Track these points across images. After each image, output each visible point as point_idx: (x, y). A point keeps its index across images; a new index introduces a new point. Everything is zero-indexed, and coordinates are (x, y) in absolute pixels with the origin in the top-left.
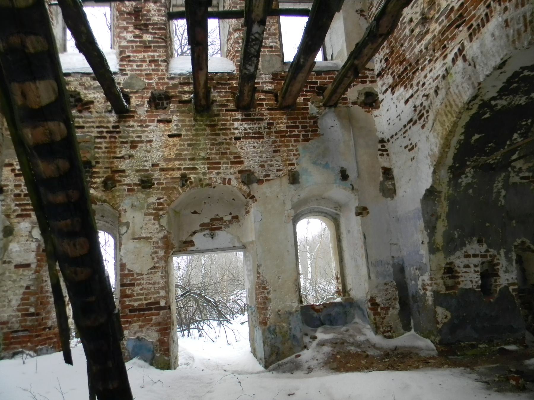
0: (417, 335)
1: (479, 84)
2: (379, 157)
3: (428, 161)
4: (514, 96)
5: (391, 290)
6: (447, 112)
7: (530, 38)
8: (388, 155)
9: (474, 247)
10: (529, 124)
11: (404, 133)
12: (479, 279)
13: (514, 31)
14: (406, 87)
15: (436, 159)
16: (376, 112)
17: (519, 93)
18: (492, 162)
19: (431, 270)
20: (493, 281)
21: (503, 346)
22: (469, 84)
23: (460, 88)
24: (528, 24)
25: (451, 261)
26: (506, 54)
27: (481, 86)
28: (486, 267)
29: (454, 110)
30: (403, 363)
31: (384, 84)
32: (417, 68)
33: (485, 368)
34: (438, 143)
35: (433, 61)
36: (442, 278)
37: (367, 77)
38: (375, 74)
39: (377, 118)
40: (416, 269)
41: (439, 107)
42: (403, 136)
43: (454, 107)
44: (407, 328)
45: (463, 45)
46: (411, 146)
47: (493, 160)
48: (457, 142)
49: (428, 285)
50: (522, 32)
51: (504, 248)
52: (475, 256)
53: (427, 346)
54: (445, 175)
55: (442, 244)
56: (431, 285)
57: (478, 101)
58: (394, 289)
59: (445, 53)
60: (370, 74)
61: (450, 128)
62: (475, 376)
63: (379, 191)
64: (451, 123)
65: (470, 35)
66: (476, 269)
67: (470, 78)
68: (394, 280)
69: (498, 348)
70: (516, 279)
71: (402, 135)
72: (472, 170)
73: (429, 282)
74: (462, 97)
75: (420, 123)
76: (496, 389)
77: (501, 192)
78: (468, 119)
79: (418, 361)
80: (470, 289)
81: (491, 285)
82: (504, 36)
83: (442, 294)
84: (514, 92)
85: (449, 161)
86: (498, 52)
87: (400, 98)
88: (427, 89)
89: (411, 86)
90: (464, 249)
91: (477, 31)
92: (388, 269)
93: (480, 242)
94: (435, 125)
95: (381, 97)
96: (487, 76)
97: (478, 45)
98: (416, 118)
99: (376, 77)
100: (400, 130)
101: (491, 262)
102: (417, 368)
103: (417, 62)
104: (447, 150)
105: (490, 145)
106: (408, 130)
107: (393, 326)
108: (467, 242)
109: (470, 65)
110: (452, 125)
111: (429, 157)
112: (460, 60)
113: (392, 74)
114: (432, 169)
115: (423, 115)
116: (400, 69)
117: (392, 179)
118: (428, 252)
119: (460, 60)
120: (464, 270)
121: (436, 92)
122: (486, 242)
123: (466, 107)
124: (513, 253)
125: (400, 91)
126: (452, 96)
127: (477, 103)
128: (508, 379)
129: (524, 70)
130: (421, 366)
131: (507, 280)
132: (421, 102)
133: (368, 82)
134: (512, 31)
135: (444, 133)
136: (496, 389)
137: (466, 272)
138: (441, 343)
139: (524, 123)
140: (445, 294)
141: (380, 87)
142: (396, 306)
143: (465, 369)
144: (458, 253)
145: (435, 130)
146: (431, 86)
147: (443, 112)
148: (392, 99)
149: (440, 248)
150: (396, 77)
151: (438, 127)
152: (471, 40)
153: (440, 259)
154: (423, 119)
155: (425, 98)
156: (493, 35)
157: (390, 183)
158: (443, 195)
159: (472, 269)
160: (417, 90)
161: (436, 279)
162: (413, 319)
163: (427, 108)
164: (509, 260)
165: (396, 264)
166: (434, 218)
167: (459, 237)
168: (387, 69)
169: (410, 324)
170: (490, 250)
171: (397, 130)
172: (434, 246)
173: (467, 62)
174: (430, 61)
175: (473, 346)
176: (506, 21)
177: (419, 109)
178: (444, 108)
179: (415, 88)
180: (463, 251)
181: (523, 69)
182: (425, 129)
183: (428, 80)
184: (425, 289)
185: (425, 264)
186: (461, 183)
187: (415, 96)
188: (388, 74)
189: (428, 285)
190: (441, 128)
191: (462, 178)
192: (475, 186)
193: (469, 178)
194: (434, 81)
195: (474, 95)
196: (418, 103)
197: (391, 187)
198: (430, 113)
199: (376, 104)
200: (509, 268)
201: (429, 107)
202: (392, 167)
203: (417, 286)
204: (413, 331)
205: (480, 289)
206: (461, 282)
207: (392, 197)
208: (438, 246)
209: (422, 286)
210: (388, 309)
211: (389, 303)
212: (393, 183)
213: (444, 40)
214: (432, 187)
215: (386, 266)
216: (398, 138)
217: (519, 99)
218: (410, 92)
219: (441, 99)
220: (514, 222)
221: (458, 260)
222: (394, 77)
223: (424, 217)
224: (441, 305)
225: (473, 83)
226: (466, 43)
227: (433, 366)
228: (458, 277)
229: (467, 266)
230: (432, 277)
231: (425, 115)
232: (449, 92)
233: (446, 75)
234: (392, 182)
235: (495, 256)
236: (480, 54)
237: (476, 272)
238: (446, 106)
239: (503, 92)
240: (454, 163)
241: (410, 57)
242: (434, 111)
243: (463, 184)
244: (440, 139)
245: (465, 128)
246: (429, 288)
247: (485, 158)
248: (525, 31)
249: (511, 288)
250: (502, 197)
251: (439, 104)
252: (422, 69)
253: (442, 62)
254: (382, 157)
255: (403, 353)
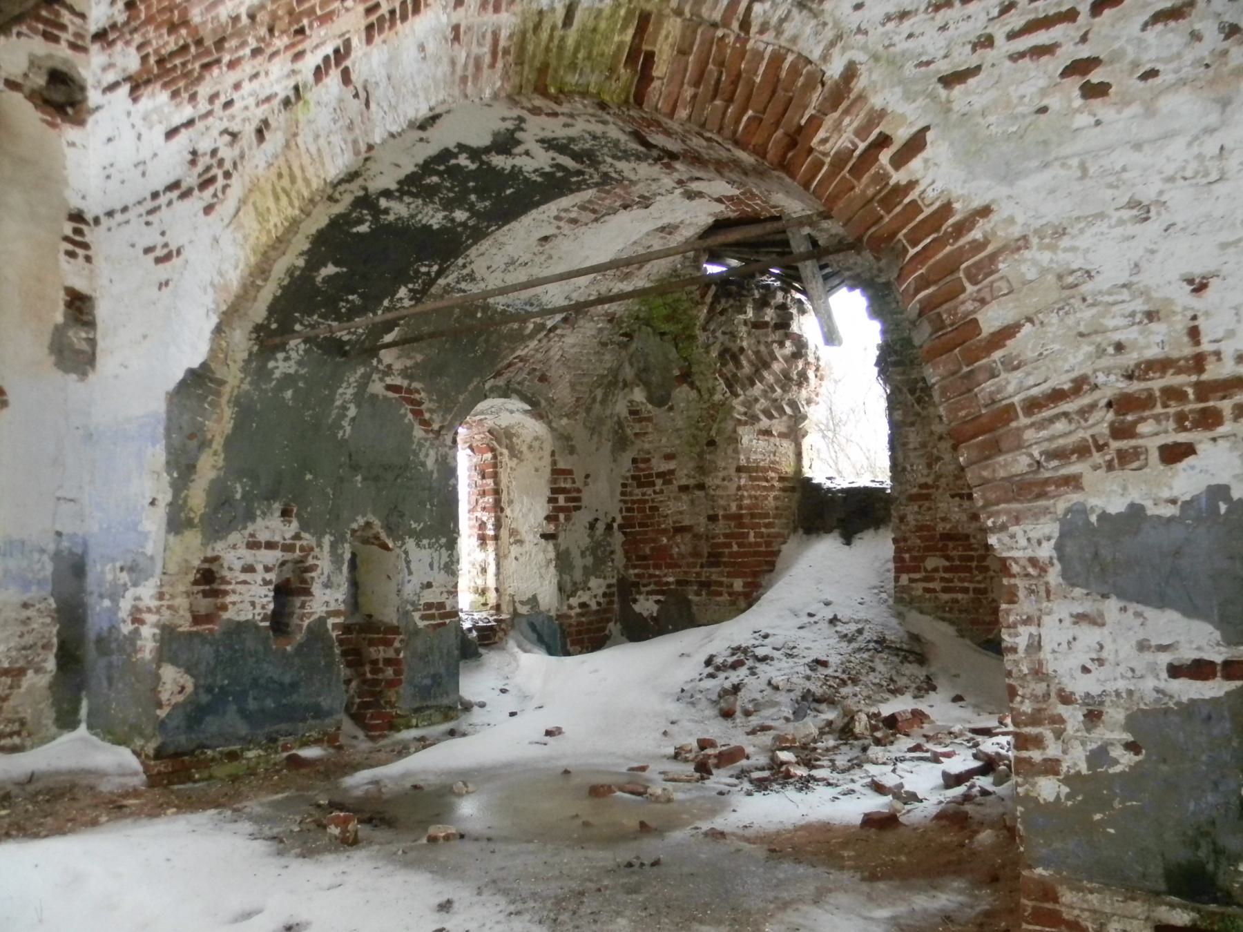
0: (94, 738)
1: (370, 147)
2: (63, 258)
3: (208, 300)
4: (425, 204)
5: (41, 620)
6: (279, 190)
7: (499, 84)
8: (88, 259)
9: (271, 526)
10: (433, 274)
11: (150, 212)
12: (270, 599)
13: (468, 56)
14: (175, 94)
15: (231, 299)
16: (71, 133)
17: (437, 200)
18: (346, 338)
19: (164, 573)
20: (298, 605)
21: (294, 752)
22: (345, 141)
23: (322, 141)
24: (500, 54)
25: (216, 553)
26: (444, 102)
27: (373, 153)
28: (288, 573)
29: (298, 192)
30: (51, 814)
31: (111, 66)
32: (215, 56)
33: (262, 805)
34: (242, 259)
35: (266, 55)
36: (188, 594)
37: (63, 27)
38: (87, 30)
39: (72, 149)
40: (122, 569)
41: (260, 171)
42: (145, 218)
43: (300, 182)
44: (67, 721)
45: (347, 44)
46: (165, 251)
47: (349, 333)
48: (288, 270)
49: (149, 610)
50: (485, 66)
51: (331, 534)
52: (270, 545)
53: (120, 765)
54: (240, 340)
55: (202, 511)
56: (158, 610)
57: (355, 189)
58: (48, 620)
59: (300, 48)
60: (73, 23)
61: (281, 230)
62: (247, 827)
63: (46, 351)
64: (286, 219)
65: (370, 28)
66: (268, 576)
67: (350, 127)
68: (52, 595)
69: (285, 754)
70: (344, 602)
71: (141, 215)
72: (302, 347)
73: (154, 603)
74: (323, 164)
75: (201, 198)
76: (298, 850)
77: (347, 409)
78: (323, 222)
79: (96, 806)
80: (247, 621)
81: (291, 614)
82: (446, 60)
83: (182, 633)
84: (428, 193)
85: (259, 311)
86: (426, 90)
87: (155, 117)
88: (238, 120)
89: (193, 97)
90: (251, 528)
91: (387, 25)
92: (37, 567)
93: (285, 513)
94: (241, 214)
95: (94, 97)
96: (392, 136)
97: (385, 57)
98: (191, 180)
99: (89, 38)
100: (139, 203)
101: (302, 562)
102: (94, 823)
103: (220, 43)
104: (259, 282)
105: (351, 297)
106: (164, 207)
107: (29, 718)
108: (258, 513)
109: (356, 96)
110: (286, 224)
111: (210, 290)
112: (334, 75)
113: (140, 47)
114: (214, 320)
115: (212, 180)
116: (167, 43)
117: (91, 324)
118: (164, 526)
119: (334, 75)
120: (243, 577)
121: (260, 133)
122: (298, 516)
123: (329, 191)
124: (347, 546)
125: (157, 98)
126: (299, 156)
127: (352, 192)
128: (322, 826)
129: (460, 152)
130: (104, 819)
131: (327, 603)
132: (213, 146)
133: (64, 44)
134: (464, 55)
135: (264, 239)
136: (298, 850)
137: (245, 582)
138: (159, 754)
139: (424, 269)
140: (190, 633)
141: (99, 71)
142: (46, 665)
143: (220, 813)
144: (235, 537)
145: (240, 226)
146: (248, 114)
147: (269, 187)
148: (129, 114)
149: (196, 521)
150: (152, 60)
151: (248, 219)
152: (369, 40)
153: (191, 549)
154: (211, 190)
155: (227, 138)
156: (422, 48)
157: (83, 335)
158: (226, 390)
159: (260, 575)
160: (209, 113)
161: (172, 597)
162: (89, 698)
163: (228, 165)
164: (336, 559)
165: (66, 553)
166: (193, 444)
167: (244, 497)
168: (126, 30)
169: (76, 710)
170: (304, 535)
171: (130, 201)
172: (182, 515)
173: (351, 88)
174: (256, 52)
175: (233, 756)
176: (456, 28)
177: (203, 162)
178: (274, 178)
179: (203, 106)
180: (246, 533)
181: (462, 148)
182: (214, 215)
183: (243, 98)
184: (138, 621)
185: (152, 558)
186: (272, 372)
187: (200, 125)
188: (127, 43)
189: (149, 610)
190: (255, 225)
191: (276, 360)
192: (301, 384)
193: (292, 363)
194: (257, 105)
195: (353, 170)
196: (204, 146)
197: (85, 346)
198: (235, 181)
199: (76, 113)
200: (333, 579)
201: (235, 164)
202: (94, 295)
203: (115, 613)
204: (82, 730)
205: (267, 624)
206: (230, 606)
207: (83, 375)
208: (192, 515)
209: (131, 614)
210: (21, 672)
211: (26, 657)
212: (91, 336)
213: (302, 14)
214: (204, 365)
215: (36, 556)
216: (127, 222)
217: (431, 213)
218: (187, 112)
219: (269, 153)
220: (359, 478)
221: (233, 553)
222: (145, 59)
223: (168, 434)
224: (174, 661)
225: (355, 142)
226: (355, 42)
227: (139, 815)
228: (225, 593)
229: (249, 569)
230: (164, 589)
231: (221, 181)
232: (293, 144)
233: (293, 99)
234: (87, 333)
235: (312, 549)
236: (385, 80)
237: (266, 582)
238: (280, 176)
239: (412, 185)
240: (268, 318)
241: (204, 23)
242: (247, 179)
243: (277, 374)
244: (248, 251)
245: (312, 243)
246: (151, 618)
247: (335, 324)
248: (492, 65)
249: (331, 622)
250: (348, 419)
251: (262, 165)
252: (232, 65)
253: (289, 66)
254: (72, 260)
255: (51, 789)
